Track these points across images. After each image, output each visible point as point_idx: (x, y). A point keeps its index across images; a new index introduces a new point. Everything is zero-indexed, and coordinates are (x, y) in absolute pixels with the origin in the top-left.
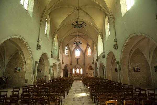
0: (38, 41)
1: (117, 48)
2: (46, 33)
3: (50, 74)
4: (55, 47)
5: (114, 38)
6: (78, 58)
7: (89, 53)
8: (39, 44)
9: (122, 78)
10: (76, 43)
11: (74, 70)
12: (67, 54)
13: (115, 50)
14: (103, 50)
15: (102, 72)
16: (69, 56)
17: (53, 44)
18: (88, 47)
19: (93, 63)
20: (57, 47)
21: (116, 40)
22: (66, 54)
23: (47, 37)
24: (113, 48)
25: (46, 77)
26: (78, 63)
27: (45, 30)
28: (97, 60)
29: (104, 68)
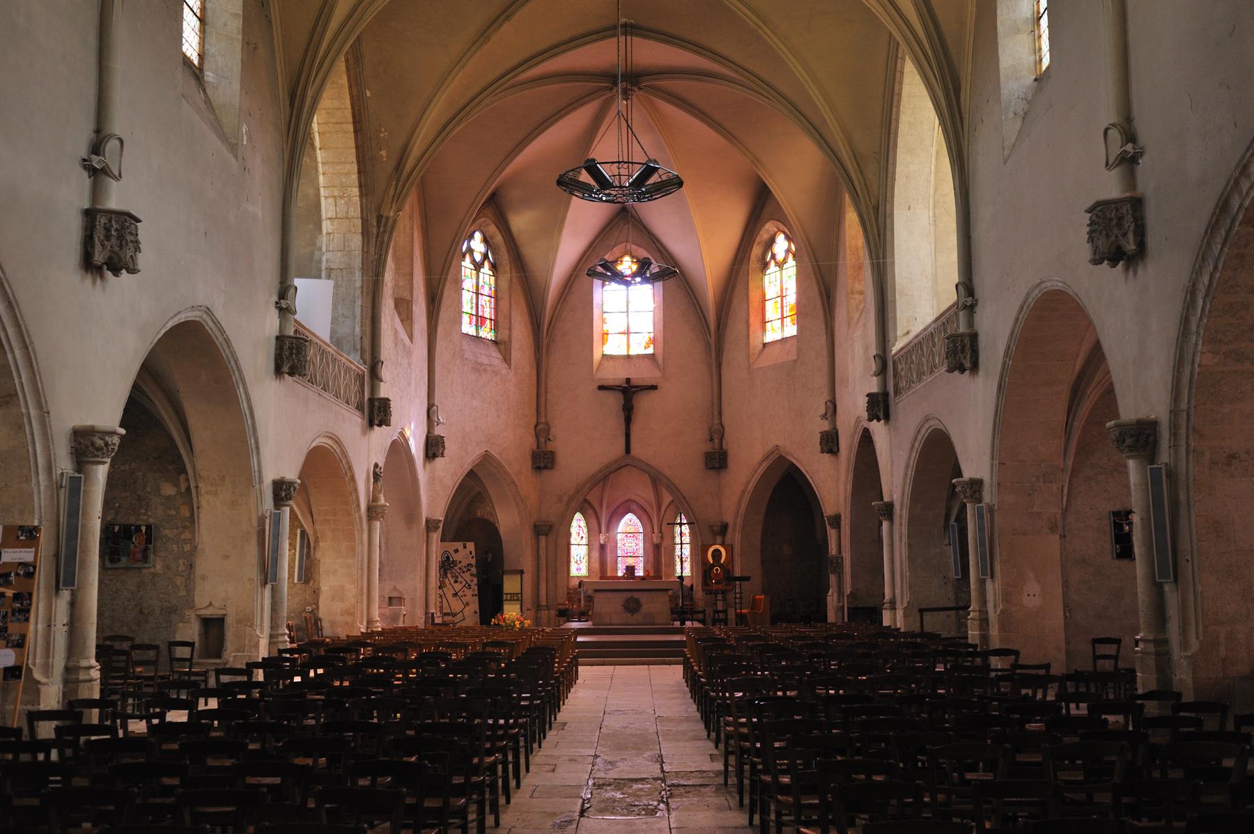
0: (96, 162)
1: (1131, 246)
2: (191, 45)
3: (275, 592)
4: (324, 240)
5: (1107, 114)
6: (642, 375)
7: (772, 311)
8: (115, 200)
9: (1184, 631)
10: (604, 183)
11: (578, 526)
12: (487, 333)
13: (1111, 274)
14: (954, 277)
15: (840, 615)
16: (516, 355)
17: (299, 205)
18: (764, 235)
19: (830, 443)
20: (356, 241)
21: (1130, 136)
22: (468, 328)
23: (208, 101)
24: (1084, 251)
25: (213, 626)
26: (636, 450)
27: (179, 19)
28: (880, 406)
29: (963, 507)
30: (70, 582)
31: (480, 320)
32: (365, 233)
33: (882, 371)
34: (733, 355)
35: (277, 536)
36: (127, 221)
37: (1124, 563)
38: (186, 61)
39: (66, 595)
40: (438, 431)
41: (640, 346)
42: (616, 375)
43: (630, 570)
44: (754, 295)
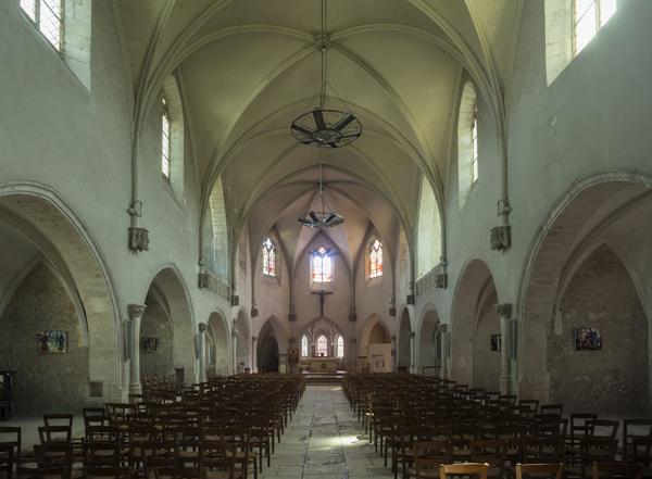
1: (506, 243)
2: (165, 170)
3: (201, 361)
7: (373, 267)
10: (316, 220)
11: (304, 340)
12: (272, 274)
15: (433, 349)
16: (282, 281)
17: (205, 228)
18: (371, 240)
19: (393, 312)
20: (226, 241)
21: (507, 205)
22: (266, 272)
25: (180, 371)
26: (326, 314)
27: (161, 138)
28: (411, 300)
30: (130, 357)
31: (270, 269)
32: (229, 239)
33: (412, 287)
34: (359, 282)
35: (201, 342)
36: (144, 232)
37: (495, 352)
38: (164, 176)
39: (128, 361)
40: (256, 307)
41: (326, 279)
42: (319, 289)
43: (322, 354)
44: (367, 262)
